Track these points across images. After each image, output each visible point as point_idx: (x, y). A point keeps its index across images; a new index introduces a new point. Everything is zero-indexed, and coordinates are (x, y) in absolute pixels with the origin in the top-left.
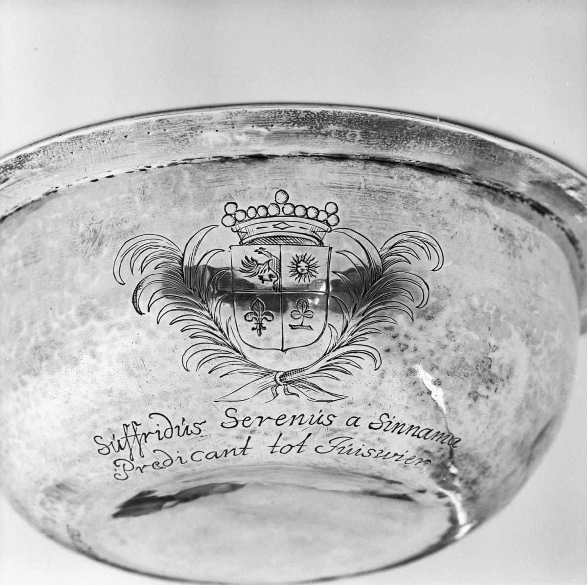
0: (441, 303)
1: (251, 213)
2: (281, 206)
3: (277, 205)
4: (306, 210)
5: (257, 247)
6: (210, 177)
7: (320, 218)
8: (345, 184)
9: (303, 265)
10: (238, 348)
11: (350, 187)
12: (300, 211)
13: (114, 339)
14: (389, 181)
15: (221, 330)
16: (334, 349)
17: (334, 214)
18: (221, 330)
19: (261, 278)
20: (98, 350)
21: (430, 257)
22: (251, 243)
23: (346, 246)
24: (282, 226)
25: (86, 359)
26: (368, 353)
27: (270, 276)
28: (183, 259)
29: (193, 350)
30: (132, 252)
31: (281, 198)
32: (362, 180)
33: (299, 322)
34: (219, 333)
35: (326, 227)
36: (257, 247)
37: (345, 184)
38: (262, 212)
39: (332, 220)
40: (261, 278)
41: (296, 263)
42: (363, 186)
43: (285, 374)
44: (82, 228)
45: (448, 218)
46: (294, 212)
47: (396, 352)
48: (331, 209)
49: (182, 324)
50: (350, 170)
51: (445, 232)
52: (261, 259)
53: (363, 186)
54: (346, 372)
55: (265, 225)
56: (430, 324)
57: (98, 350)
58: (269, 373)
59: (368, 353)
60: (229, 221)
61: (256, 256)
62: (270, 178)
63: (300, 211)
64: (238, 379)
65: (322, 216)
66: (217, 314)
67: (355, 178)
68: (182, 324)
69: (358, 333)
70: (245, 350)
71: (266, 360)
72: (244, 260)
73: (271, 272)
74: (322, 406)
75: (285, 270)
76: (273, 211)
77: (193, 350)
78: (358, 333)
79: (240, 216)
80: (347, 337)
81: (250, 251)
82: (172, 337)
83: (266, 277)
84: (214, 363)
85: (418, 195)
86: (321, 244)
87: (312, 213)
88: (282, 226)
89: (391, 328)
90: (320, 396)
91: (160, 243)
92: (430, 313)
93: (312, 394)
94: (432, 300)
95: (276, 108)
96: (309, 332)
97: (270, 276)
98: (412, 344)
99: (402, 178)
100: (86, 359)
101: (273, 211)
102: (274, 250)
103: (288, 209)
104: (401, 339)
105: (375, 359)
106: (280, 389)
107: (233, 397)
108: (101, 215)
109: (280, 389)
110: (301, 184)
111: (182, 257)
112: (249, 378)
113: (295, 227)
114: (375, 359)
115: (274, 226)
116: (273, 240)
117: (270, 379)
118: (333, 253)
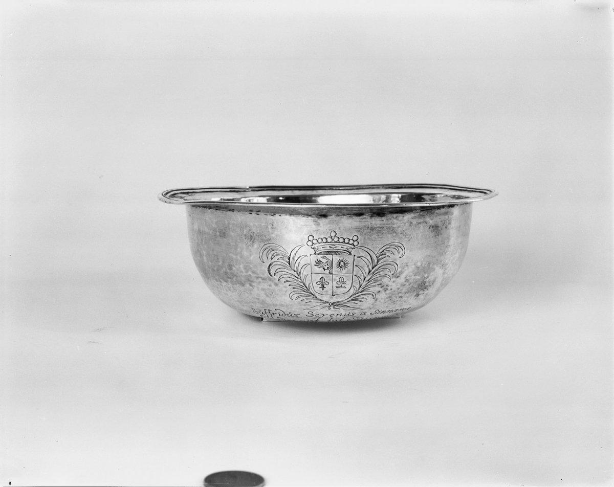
0: (403, 270)
1: (320, 241)
2: (333, 238)
3: (331, 237)
4: (344, 239)
5: (322, 256)
6: (302, 223)
7: (350, 243)
8: (361, 227)
9: (342, 263)
10: (312, 293)
11: (364, 227)
12: (341, 240)
13: (260, 282)
14: (382, 222)
15: (306, 287)
16: (355, 294)
17: (356, 240)
18: (306, 287)
19: (324, 268)
20: (253, 284)
21: (399, 252)
22: (320, 253)
23: (362, 254)
24: (333, 247)
25: (247, 285)
26: (370, 294)
27: (328, 268)
28: (290, 258)
29: (294, 293)
30: (267, 250)
31: (333, 234)
32: (369, 224)
33: (340, 285)
34: (305, 288)
35: (353, 247)
36: (322, 256)
37: (361, 227)
38: (324, 240)
39: (356, 243)
40: (324, 268)
41: (339, 262)
42: (370, 226)
43: (334, 303)
44: (245, 232)
45: (407, 232)
46: (339, 240)
47: (383, 292)
48: (355, 238)
49: (289, 283)
50: (364, 220)
51: (407, 239)
52: (324, 261)
53: (370, 226)
54: (360, 301)
55: (326, 246)
56: (398, 279)
57: (253, 284)
58: (327, 302)
59: (370, 294)
60: (310, 243)
61: (322, 259)
62: (329, 226)
63: (341, 240)
64: (314, 304)
65: (351, 242)
66: (305, 281)
67: (366, 223)
68: (289, 283)
69: (366, 288)
70: (317, 295)
71: (325, 299)
72: (317, 261)
73: (328, 266)
74: (350, 311)
75: (334, 265)
76: (329, 240)
77: (294, 293)
78: (366, 288)
79: (315, 242)
80: (361, 290)
81: (319, 257)
82: (285, 287)
83: (326, 268)
84: (303, 298)
85: (395, 226)
86: (350, 254)
87: (346, 241)
88: (333, 247)
89: (380, 284)
90: (349, 308)
91: (280, 249)
92: (398, 275)
93: (345, 308)
94: (399, 270)
95: (330, 206)
96: (344, 289)
97: (328, 268)
98: (389, 288)
99: (388, 220)
100: (247, 285)
101: (329, 240)
102: (330, 257)
103: (336, 239)
104: (385, 287)
105: (373, 295)
106: (332, 308)
107: (311, 309)
108: (254, 229)
109: (332, 308)
110: (342, 228)
111: (288, 261)
112: (317, 304)
113: (339, 247)
114: (373, 295)
115: (330, 247)
116: (329, 253)
117: (327, 304)
118: (356, 258)
